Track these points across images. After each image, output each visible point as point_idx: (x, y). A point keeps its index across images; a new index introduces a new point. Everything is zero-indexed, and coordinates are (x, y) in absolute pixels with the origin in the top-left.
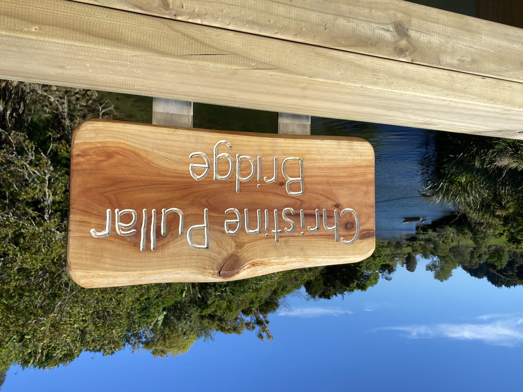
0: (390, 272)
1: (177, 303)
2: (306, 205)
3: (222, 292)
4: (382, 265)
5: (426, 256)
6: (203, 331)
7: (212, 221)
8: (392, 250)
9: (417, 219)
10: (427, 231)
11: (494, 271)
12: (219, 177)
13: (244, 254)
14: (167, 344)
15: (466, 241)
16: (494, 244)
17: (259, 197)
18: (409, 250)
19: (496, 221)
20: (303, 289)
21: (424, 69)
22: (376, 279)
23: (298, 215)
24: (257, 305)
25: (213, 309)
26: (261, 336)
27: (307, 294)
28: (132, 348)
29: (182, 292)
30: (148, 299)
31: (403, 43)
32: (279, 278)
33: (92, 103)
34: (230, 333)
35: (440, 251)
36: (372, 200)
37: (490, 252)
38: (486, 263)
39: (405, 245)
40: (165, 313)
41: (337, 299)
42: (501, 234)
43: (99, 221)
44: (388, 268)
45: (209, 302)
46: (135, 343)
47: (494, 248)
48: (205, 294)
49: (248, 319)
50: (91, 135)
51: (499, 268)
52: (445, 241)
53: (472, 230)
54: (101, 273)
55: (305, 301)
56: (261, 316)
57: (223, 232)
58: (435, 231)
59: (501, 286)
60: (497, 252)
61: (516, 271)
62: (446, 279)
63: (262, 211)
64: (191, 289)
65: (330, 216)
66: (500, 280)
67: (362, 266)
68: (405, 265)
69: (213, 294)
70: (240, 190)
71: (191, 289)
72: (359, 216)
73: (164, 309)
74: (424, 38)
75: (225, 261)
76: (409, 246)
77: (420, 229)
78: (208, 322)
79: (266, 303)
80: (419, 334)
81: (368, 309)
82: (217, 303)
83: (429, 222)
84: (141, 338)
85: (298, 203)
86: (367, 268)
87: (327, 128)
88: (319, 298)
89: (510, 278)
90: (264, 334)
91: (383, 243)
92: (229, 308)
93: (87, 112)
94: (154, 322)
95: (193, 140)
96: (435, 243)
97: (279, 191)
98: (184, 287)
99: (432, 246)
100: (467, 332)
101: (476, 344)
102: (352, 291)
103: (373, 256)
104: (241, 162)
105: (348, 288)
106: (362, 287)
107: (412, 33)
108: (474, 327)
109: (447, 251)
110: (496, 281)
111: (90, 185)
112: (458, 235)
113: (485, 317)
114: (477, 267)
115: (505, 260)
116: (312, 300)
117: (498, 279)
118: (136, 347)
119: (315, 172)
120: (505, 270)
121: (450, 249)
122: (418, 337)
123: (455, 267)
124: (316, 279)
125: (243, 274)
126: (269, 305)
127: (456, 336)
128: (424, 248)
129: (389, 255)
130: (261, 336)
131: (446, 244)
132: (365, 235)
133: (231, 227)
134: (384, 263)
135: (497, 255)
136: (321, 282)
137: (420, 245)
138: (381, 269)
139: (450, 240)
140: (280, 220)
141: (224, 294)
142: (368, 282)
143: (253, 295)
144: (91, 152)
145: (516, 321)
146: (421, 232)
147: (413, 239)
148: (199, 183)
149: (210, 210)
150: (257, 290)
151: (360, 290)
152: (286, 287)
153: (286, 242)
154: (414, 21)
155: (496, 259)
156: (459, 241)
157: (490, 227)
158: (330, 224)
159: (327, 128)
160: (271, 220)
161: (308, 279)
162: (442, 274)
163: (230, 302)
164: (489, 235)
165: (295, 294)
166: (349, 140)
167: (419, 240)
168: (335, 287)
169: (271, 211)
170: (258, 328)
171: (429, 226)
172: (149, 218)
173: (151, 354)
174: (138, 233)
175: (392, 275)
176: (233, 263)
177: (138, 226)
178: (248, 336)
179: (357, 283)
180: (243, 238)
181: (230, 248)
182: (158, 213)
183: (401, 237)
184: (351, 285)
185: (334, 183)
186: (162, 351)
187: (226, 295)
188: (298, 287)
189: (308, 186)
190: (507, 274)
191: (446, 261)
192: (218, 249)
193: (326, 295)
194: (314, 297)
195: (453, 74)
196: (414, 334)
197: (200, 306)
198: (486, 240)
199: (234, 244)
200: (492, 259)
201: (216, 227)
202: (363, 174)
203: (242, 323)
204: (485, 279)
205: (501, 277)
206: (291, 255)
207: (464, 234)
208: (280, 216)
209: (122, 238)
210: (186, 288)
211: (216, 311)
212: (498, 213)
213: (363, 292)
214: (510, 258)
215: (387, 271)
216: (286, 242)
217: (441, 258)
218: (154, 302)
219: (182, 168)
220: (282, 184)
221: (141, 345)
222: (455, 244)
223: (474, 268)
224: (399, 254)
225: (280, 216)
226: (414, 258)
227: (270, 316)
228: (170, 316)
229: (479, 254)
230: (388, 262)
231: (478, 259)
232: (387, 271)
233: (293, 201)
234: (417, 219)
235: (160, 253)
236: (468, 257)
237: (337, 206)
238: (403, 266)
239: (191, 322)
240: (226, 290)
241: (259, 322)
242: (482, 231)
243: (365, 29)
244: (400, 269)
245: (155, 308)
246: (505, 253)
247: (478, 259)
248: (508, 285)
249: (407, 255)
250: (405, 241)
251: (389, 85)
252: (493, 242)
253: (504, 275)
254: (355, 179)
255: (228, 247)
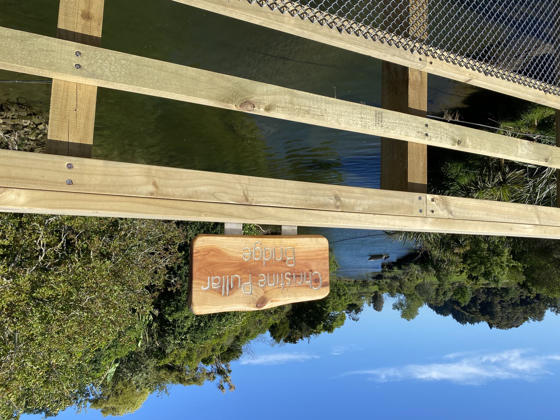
0: (357, 312)
1: (132, 353)
2: (296, 271)
3: (182, 340)
4: (349, 305)
5: (392, 295)
6: (159, 383)
7: (252, 281)
8: (359, 289)
9: (380, 256)
10: (393, 269)
11: (459, 309)
12: (256, 259)
13: (268, 296)
14: (120, 401)
15: (431, 279)
16: (457, 280)
17: (274, 268)
18: (375, 288)
19: (456, 258)
20: (268, 333)
21: (347, 214)
22: (343, 319)
23: (292, 276)
24: (218, 353)
25: (171, 359)
26: (221, 387)
27: (272, 338)
28: (77, 407)
29: (138, 342)
30: (99, 350)
31: (338, 203)
32: (243, 323)
33: (41, 137)
34: (190, 384)
35: (405, 289)
36: (327, 267)
37: (454, 289)
38: (451, 299)
39: (371, 284)
40: (117, 365)
41: (302, 343)
42: (462, 272)
43: (205, 283)
44: (354, 308)
45: (168, 351)
46: (81, 401)
47: (457, 284)
48: (163, 343)
49: (209, 368)
50: (202, 243)
51: (463, 305)
52: (411, 279)
53: (435, 267)
54: (206, 307)
55: (270, 346)
56: (223, 366)
57: (258, 286)
58: (400, 268)
59: (466, 323)
60: (460, 290)
61: (479, 307)
62: (413, 317)
63: (276, 275)
64: (147, 337)
65: (307, 276)
66: (464, 317)
67: (328, 307)
68: (372, 305)
69: (172, 342)
70: (265, 265)
71: (147, 337)
72: (321, 276)
73: (116, 362)
74: (347, 200)
75: (260, 300)
76: (375, 284)
77: (385, 266)
78: (165, 374)
79: (227, 351)
80: (388, 377)
81: (335, 352)
82: (176, 352)
83: (395, 260)
84: (88, 395)
85: (292, 270)
86: (333, 309)
87: (303, 231)
88: (284, 343)
89: (474, 314)
90: (225, 385)
91: (349, 281)
92: (189, 357)
93: (35, 146)
94: (105, 376)
95: (244, 242)
96: (400, 281)
97: (284, 265)
98: (140, 336)
99: (398, 284)
100: (435, 373)
101: (444, 386)
102: (319, 333)
103: (329, 295)
104: (265, 251)
105: (315, 331)
106: (329, 329)
107: (342, 199)
108: (441, 366)
109: (413, 289)
110: (460, 318)
111: (201, 266)
112: (422, 273)
113: (451, 356)
114: (442, 304)
115: (468, 298)
116: (277, 345)
117: (462, 315)
118: (83, 406)
119: (301, 254)
120: (469, 306)
121: (416, 287)
122: (387, 381)
123: (421, 305)
124: (282, 323)
125: (268, 306)
126: (232, 352)
127: (424, 376)
128: (390, 286)
129: (355, 294)
130: (221, 387)
131: (411, 281)
132: (324, 285)
133: (261, 283)
134: (350, 303)
135: (461, 292)
136: (287, 325)
137: (386, 283)
138: (348, 309)
139: (415, 278)
140: (284, 279)
141: (184, 342)
142: (334, 323)
143: (215, 342)
144: (201, 251)
145: (481, 358)
146: (387, 269)
147: (379, 277)
148: (247, 263)
149: (252, 275)
150: (220, 336)
151: (326, 332)
152: (250, 332)
153: (287, 290)
154: (343, 194)
155: (459, 296)
156: (424, 278)
157: (452, 264)
158: (307, 280)
159: (303, 231)
160: (280, 279)
161: (273, 322)
162: (408, 313)
163: (190, 350)
164: (451, 272)
165: (259, 339)
166: (316, 237)
167: (385, 278)
168: (302, 329)
169: (280, 274)
170: (219, 378)
171: (395, 264)
172: (226, 280)
173: (101, 413)
174: (221, 288)
175: (359, 315)
176: (263, 301)
177: (221, 285)
178: (209, 386)
179: (324, 325)
180: (268, 289)
181: (261, 293)
182: (230, 278)
183: (367, 275)
184: (318, 327)
185: (309, 259)
186: (113, 409)
187: (187, 343)
188: (262, 331)
189: (297, 261)
190: (471, 311)
191: (412, 300)
192: (256, 294)
193: (291, 339)
194: (278, 341)
195: (361, 214)
196: (383, 377)
197: (156, 357)
198: (449, 277)
199: (263, 292)
200: (456, 295)
201: (255, 283)
202: (323, 254)
203: (203, 373)
204: (450, 316)
205: (465, 314)
206: (289, 296)
207: (428, 271)
208: (284, 277)
209: (214, 290)
210: (142, 337)
211: (174, 361)
212: (456, 251)
213: (330, 334)
214: (473, 294)
215: (354, 311)
216: (287, 290)
217: (408, 296)
218: (105, 354)
219: (240, 256)
220: (285, 261)
221: (89, 404)
222: (420, 281)
223: (439, 306)
224: (366, 292)
225: (284, 277)
226: (381, 297)
227: (232, 364)
228: (123, 369)
229: (444, 291)
230: (355, 302)
231: (443, 297)
232: (354, 311)
233: (290, 269)
234: (380, 256)
235: (230, 297)
236: (433, 294)
237: (311, 271)
238: (370, 306)
239: (147, 374)
240: (186, 337)
241: (220, 372)
242: (445, 269)
243: (322, 199)
244: (367, 309)
245: (106, 360)
246: (468, 289)
247: (443, 297)
248: (472, 322)
249: (374, 294)
250: (371, 279)
251: (332, 222)
252: (455, 278)
253: (468, 312)
254: (319, 257)
255: (261, 293)
